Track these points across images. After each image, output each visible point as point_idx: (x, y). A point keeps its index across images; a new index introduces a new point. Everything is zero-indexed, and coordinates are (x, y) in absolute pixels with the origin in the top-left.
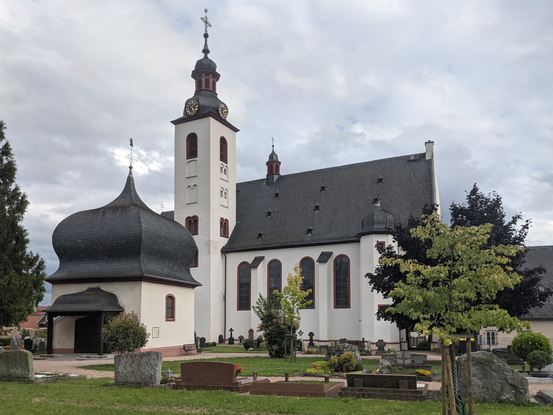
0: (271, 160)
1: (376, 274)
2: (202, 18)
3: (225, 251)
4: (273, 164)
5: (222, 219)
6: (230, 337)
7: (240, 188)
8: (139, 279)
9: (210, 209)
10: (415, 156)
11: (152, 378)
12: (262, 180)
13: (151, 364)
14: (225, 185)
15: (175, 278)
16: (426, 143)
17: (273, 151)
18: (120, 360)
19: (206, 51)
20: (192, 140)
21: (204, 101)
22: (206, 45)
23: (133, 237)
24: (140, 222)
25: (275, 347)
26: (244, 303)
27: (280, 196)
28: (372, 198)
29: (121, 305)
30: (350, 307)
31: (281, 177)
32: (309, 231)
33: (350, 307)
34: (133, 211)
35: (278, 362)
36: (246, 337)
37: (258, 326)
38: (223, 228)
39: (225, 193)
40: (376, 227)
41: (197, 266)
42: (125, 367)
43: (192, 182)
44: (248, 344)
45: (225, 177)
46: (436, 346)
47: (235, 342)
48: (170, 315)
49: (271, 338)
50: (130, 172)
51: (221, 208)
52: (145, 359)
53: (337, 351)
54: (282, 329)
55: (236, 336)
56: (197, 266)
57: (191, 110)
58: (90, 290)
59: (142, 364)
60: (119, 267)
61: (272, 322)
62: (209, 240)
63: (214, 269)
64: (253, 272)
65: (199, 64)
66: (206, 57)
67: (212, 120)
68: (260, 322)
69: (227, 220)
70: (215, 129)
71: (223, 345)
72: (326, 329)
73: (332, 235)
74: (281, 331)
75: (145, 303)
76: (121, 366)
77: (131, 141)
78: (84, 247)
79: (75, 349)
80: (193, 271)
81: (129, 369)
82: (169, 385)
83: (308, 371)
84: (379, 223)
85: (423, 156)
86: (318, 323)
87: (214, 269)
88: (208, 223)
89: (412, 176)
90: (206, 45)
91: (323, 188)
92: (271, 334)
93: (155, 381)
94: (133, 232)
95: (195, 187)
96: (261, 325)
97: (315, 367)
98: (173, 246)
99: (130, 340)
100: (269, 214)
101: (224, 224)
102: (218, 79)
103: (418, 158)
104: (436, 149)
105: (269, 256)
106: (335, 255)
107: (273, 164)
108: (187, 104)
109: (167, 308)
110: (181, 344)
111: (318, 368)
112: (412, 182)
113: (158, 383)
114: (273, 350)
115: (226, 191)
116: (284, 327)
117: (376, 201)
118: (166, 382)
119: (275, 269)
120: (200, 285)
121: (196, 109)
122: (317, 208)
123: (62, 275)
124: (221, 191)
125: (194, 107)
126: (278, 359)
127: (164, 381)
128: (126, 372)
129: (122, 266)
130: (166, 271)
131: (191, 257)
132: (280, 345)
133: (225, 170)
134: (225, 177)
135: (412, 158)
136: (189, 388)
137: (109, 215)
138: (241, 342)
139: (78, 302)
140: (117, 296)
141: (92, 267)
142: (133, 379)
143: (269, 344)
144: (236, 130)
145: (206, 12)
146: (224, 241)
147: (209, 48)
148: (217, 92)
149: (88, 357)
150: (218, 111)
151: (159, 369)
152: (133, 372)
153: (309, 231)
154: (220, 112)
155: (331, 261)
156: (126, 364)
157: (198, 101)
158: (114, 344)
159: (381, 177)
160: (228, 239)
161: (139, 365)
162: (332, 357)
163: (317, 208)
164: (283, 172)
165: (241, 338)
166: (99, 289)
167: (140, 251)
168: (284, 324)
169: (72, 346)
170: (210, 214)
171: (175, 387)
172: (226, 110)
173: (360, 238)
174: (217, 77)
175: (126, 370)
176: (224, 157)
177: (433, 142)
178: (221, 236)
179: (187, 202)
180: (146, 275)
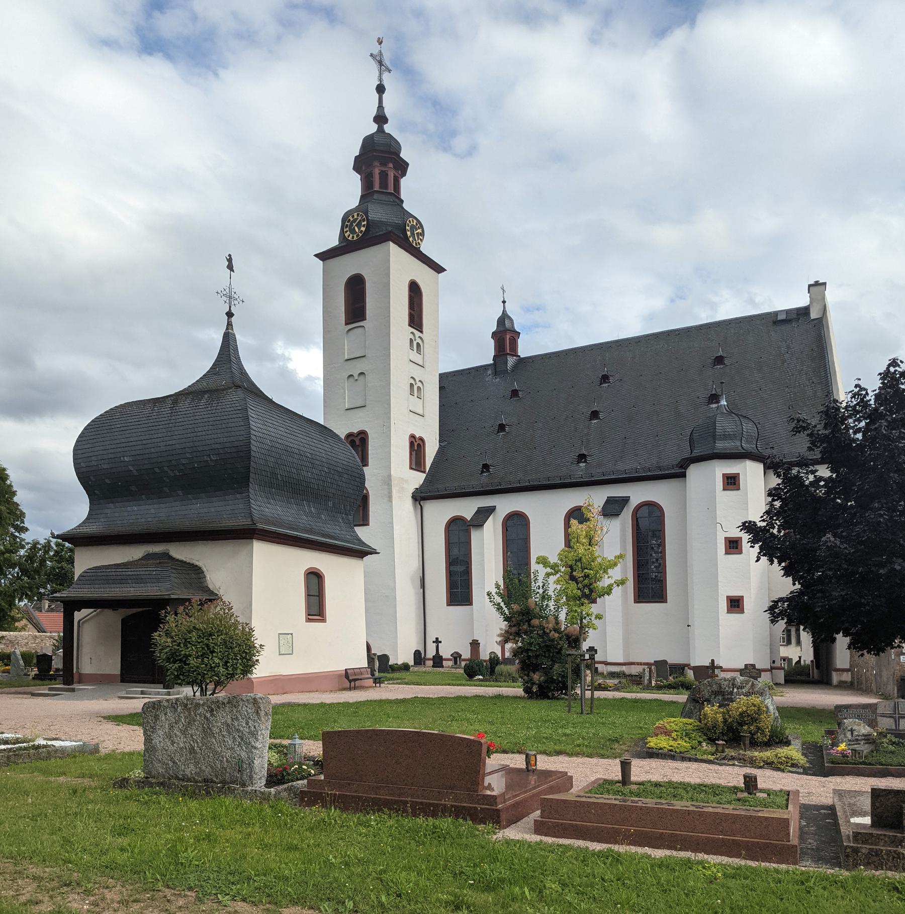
0: (502, 329)
1: (764, 524)
2: (372, 55)
3: (420, 497)
4: (505, 336)
5: (413, 436)
6: (434, 653)
7: (447, 381)
8: (247, 534)
9: (389, 418)
10: (788, 312)
11: (243, 768)
12: (485, 367)
13: (238, 731)
14: (418, 373)
15: (323, 536)
16: (810, 286)
17: (504, 312)
18: (156, 717)
19: (381, 119)
20: (356, 289)
21: (377, 213)
22: (381, 107)
23: (234, 450)
24: (247, 418)
25: (536, 677)
26: (459, 591)
27: (520, 394)
28: (704, 395)
29: (211, 587)
30: (666, 602)
31: (523, 361)
32: (582, 457)
33: (666, 602)
34: (235, 397)
35: (539, 709)
36: (466, 654)
37: (499, 632)
38: (414, 453)
39: (419, 388)
40: (720, 445)
41: (368, 524)
42: (169, 736)
43: (356, 368)
44: (476, 668)
45: (418, 358)
46: (847, 677)
47: (444, 663)
48: (316, 609)
49: (529, 657)
50: (229, 325)
51: (410, 418)
52: (223, 716)
53: (716, 693)
54: (553, 640)
55: (445, 653)
56: (368, 524)
57: (352, 231)
58: (148, 557)
59: (216, 730)
60: (206, 510)
61: (530, 625)
62: (390, 476)
63: (402, 525)
64: (475, 535)
65: (369, 144)
66: (380, 130)
67: (393, 247)
68: (504, 625)
69: (421, 439)
70: (400, 266)
71: (421, 669)
72: (621, 641)
73: (628, 466)
74: (548, 643)
75: (262, 586)
76: (161, 732)
77: (230, 260)
78: (135, 473)
79: (122, 675)
80: (361, 532)
81: (181, 741)
82: (289, 790)
83: (653, 742)
84: (726, 437)
85: (804, 312)
86: (618, 631)
87: (402, 525)
88: (387, 444)
89: (783, 350)
90: (381, 107)
91: (605, 378)
92: (527, 651)
93: (251, 777)
94: (232, 439)
95: (362, 377)
96: (507, 632)
97: (667, 733)
98: (318, 472)
99: (217, 661)
100: (502, 427)
101: (417, 446)
102: (404, 174)
103: (795, 316)
104: (831, 296)
105: (505, 505)
106: (635, 502)
107: (505, 336)
108: (344, 219)
109: (309, 595)
110: (342, 667)
111: (674, 734)
112: (784, 361)
113: (260, 784)
114: (533, 684)
115: (420, 384)
116: (557, 635)
117: (714, 398)
118: (281, 782)
119: (517, 530)
120: (373, 552)
121: (363, 229)
122: (595, 415)
123: (94, 529)
124: (412, 385)
125: (359, 225)
126: (545, 703)
127: (275, 778)
128: (172, 748)
129: (213, 510)
130: (304, 520)
131: (358, 508)
132: (546, 672)
133: (418, 344)
134: (418, 358)
135: (781, 317)
136: (346, 804)
137: (184, 405)
138: (456, 663)
139: (122, 581)
140: (204, 569)
141: (152, 511)
142: (190, 770)
143: (522, 669)
144: (439, 269)
145: (380, 43)
146: (418, 479)
147: (388, 112)
148: (402, 197)
149: (142, 693)
150: (405, 231)
151: (263, 741)
152: (192, 751)
153: (582, 457)
154: (409, 233)
155: (627, 514)
156: (171, 727)
157: (366, 213)
158: (181, 668)
159: (721, 353)
160: (424, 475)
161: (207, 732)
162: (708, 709)
163: (595, 415)
164: (527, 348)
165: (456, 657)
166: (167, 555)
167: (248, 478)
168: (555, 630)
169: (117, 671)
170: (390, 427)
171: (309, 798)
172: (420, 231)
173: (686, 468)
174: (402, 167)
175: (173, 743)
176: (415, 320)
177: (825, 284)
178: (411, 468)
179: (347, 407)
180: (260, 526)
